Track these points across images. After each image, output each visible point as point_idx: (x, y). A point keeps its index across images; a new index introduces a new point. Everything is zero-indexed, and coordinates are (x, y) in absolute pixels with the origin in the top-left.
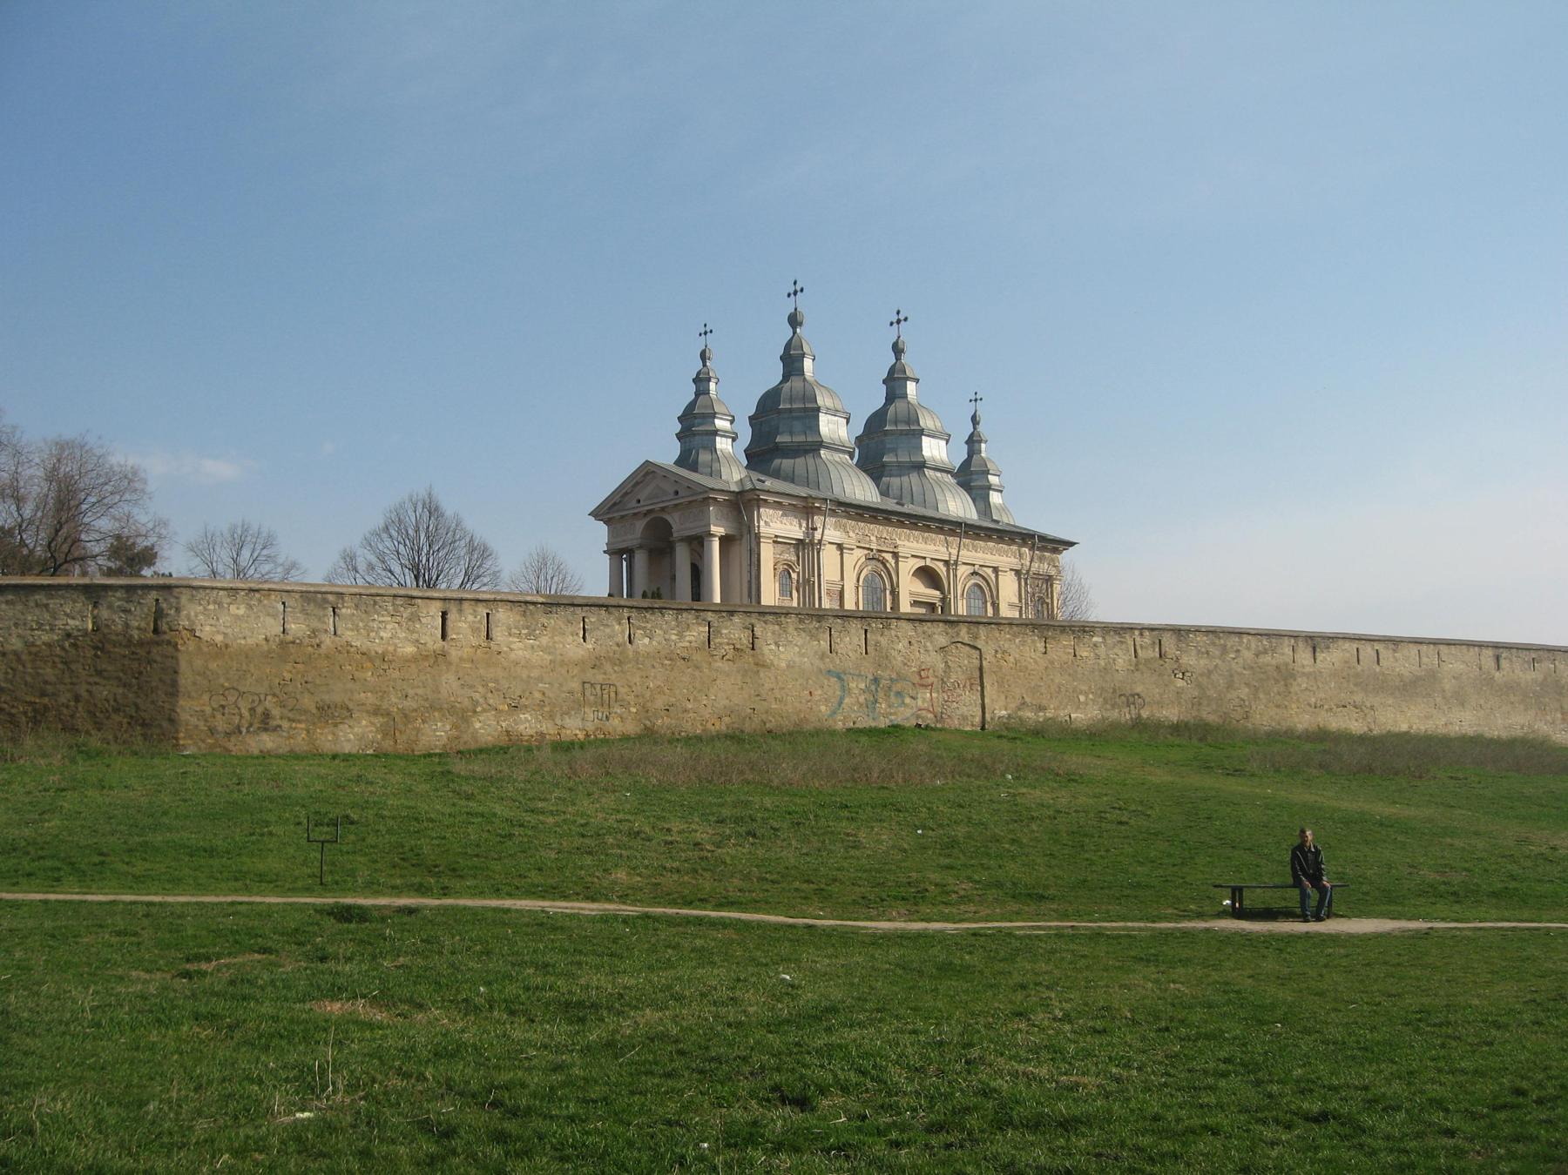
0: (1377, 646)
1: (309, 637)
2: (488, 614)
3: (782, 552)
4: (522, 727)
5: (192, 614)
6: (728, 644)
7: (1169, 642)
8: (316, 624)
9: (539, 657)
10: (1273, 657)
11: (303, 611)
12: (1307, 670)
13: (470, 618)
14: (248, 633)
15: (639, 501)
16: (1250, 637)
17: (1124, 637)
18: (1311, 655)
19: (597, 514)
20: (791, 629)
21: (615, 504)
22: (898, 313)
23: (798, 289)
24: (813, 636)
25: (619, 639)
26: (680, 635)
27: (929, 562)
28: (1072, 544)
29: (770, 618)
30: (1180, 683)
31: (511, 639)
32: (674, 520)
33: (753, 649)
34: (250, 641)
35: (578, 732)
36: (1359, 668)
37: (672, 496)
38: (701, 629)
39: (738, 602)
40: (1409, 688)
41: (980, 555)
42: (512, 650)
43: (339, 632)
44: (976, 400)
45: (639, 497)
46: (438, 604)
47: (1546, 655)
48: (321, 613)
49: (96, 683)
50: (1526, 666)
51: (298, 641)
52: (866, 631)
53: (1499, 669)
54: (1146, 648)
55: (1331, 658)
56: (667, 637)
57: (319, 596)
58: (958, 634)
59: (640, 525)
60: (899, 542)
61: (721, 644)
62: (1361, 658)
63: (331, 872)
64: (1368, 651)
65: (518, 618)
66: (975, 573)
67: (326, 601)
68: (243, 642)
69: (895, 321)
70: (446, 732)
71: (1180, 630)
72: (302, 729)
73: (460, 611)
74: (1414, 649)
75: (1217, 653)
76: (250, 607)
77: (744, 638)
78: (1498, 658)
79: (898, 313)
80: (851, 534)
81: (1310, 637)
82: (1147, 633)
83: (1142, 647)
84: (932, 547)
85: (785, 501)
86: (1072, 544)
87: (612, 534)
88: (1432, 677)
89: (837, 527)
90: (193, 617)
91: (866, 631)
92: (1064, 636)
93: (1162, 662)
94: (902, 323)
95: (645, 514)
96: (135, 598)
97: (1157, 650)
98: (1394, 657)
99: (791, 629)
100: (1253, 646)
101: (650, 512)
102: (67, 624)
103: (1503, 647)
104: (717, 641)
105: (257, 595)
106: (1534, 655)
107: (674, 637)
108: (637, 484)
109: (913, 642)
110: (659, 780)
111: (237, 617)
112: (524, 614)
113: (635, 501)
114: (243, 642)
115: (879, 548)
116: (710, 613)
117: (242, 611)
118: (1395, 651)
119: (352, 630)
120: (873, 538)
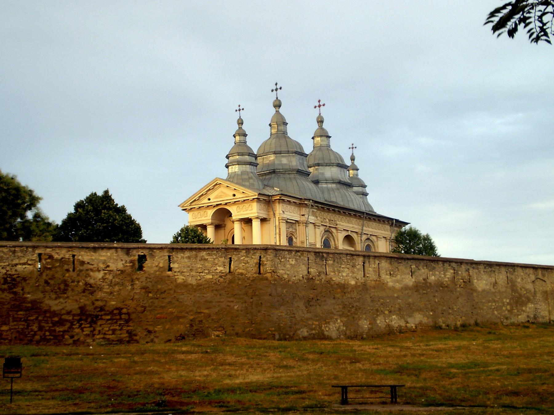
3: (289, 227)
6: (461, 279)
8: (320, 269)
9: (398, 286)
13: (373, 266)
14: (296, 274)
15: (209, 199)
22: (319, 101)
27: (349, 233)
32: (233, 209)
33: (470, 282)
41: (370, 229)
43: (328, 273)
44: (353, 148)
45: (209, 197)
49: (233, 302)
51: (314, 278)
59: (211, 212)
60: (338, 223)
66: (368, 239)
67: (323, 256)
69: (238, 109)
70: (368, 325)
72: (29, 293)
76: (296, 260)
79: (319, 101)
80: (319, 218)
84: (351, 225)
85: (292, 200)
89: (314, 214)
95: (214, 206)
101: (217, 205)
104: (457, 277)
110: (318, 331)
112: (390, 263)
113: (207, 198)
114: (294, 278)
115: (330, 226)
120: (327, 220)
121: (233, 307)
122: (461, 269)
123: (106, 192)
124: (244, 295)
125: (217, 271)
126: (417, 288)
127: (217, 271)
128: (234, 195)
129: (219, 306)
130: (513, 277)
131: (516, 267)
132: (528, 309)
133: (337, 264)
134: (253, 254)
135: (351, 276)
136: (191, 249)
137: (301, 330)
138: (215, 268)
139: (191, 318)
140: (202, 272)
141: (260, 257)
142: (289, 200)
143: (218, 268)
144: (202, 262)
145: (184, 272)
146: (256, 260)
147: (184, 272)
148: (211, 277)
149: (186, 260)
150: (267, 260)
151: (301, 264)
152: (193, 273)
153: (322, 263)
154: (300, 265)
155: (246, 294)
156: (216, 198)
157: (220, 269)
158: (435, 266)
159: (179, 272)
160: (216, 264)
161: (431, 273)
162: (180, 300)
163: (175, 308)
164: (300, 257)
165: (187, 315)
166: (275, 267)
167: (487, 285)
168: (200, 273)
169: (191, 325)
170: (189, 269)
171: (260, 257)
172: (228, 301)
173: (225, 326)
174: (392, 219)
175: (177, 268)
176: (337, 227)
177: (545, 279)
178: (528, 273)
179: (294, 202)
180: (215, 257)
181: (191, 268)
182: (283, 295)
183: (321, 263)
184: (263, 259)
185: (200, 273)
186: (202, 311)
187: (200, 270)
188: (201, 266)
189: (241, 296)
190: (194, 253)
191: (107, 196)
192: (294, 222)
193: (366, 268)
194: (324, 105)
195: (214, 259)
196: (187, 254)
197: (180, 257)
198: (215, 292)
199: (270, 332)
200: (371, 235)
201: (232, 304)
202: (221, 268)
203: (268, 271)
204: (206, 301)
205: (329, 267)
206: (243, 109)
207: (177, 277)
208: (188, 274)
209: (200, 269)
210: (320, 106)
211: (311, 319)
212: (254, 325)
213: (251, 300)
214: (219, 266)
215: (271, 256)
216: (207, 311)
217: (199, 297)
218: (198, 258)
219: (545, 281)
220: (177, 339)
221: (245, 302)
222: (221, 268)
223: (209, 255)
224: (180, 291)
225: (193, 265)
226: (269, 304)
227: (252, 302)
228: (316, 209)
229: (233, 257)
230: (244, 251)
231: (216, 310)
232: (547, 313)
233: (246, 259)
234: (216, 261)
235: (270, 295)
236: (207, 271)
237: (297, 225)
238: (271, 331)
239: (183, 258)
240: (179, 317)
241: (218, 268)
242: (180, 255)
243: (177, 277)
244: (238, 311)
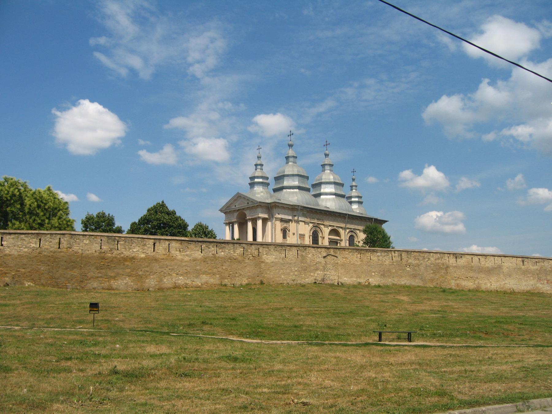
0: (479, 257)
1: (110, 251)
2: (169, 244)
4: (180, 282)
5: (71, 243)
6: (250, 254)
7: (404, 255)
8: (112, 247)
9: (187, 259)
10: (441, 260)
11: (108, 242)
12: (454, 265)
13: (164, 245)
14: (90, 249)
15: (236, 206)
16: (433, 254)
17: (388, 254)
18: (455, 260)
19: (221, 210)
20: (272, 250)
21: (228, 207)
22: (326, 142)
23: (292, 134)
24: (280, 253)
25: (213, 252)
26: (234, 252)
27: (335, 228)
28: (386, 221)
29: (265, 246)
30: (408, 269)
31: (177, 252)
32: (247, 212)
34: (90, 252)
35: (199, 283)
36: (473, 264)
37: (247, 205)
38: (241, 249)
39: (270, 241)
40: (489, 271)
42: (177, 256)
46: (153, 240)
47: (541, 260)
48: (114, 243)
49: (40, 265)
50: (534, 264)
52: (298, 251)
53: (523, 265)
54: (396, 257)
55: (462, 261)
56: (229, 252)
57: (113, 237)
58: (330, 252)
59: (236, 214)
61: (248, 255)
62: (473, 261)
63: (479, 357)
64: (476, 259)
65: (179, 245)
67: (115, 239)
68: (88, 252)
71: (408, 251)
73: (160, 243)
74: (492, 258)
75: (422, 259)
77: (256, 253)
78: (523, 261)
79: (326, 142)
81: (455, 254)
82: (396, 252)
83: (395, 257)
86: (386, 221)
87: (227, 218)
88: (500, 267)
90: (71, 244)
91: (298, 251)
92: (367, 253)
93: (401, 262)
94: (328, 145)
96: (53, 237)
97: (400, 258)
98: (485, 261)
99: (272, 250)
100: (435, 257)
102: (31, 246)
103: (525, 258)
105: (93, 237)
106: (537, 260)
107: (232, 252)
108: (235, 200)
109: (314, 254)
111: (86, 244)
113: (234, 206)
114: (88, 252)
116: (244, 244)
117: (87, 242)
118: (485, 258)
119: (124, 249)
121: (41, 268)
122: (251, 248)
123: (163, 202)
124: (48, 261)
125: (31, 247)
126: (204, 260)
127: (31, 247)
128: (248, 203)
129: (31, 267)
130: (304, 254)
131: (307, 248)
132: (316, 275)
133: (128, 244)
134: (55, 237)
135: (142, 251)
136: (15, 234)
137: (92, 283)
138: (30, 245)
139: (13, 274)
140: (21, 247)
141: (60, 238)
142: (282, 206)
143: (32, 245)
144: (22, 241)
145: (10, 247)
146: (57, 241)
147: (10, 247)
148: (27, 250)
149: (11, 240)
150: (65, 241)
151: (94, 243)
152: (16, 248)
153: (114, 243)
154: (93, 244)
155: (49, 260)
156: (239, 205)
157: (33, 245)
158: (225, 246)
159: (7, 246)
160: (31, 243)
161: (221, 250)
162: (7, 263)
163: (3, 267)
164: (93, 239)
165: (11, 272)
166: (70, 245)
167: (276, 258)
168: (20, 247)
169: (13, 278)
170: (13, 245)
171: (60, 238)
172: (37, 265)
173: (35, 279)
174: (372, 219)
175: (6, 244)
176: (324, 223)
177: (336, 255)
178: (320, 251)
179: (281, 207)
180: (30, 238)
181: (14, 244)
182: (76, 262)
183: (113, 243)
184: (62, 240)
185: (20, 247)
186: (20, 270)
187: (20, 246)
188: (21, 243)
189: (46, 262)
190: (17, 235)
191: (163, 205)
192: (288, 220)
193: (156, 246)
194: (329, 144)
195: (29, 239)
196: (13, 236)
197: (8, 238)
198: (29, 259)
199: (65, 284)
200: (354, 229)
201: (39, 267)
202: (34, 245)
203: (65, 247)
204: (23, 264)
205: (120, 245)
206: (261, 148)
207: (5, 250)
208: (13, 248)
209: (20, 245)
210: (327, 145)
211: (101, 277)
212: (54, 279)
213: (53, 264)
214: (33, 244)
215: (67, 238)
216: (23, 270)
217: (19, 262)
218: (19, 239)
219: (337, 257)
220: (4, 286)
221: (49, 266)
222: (34, 245)
223: (26, 237)
224: (6, 258)
225: (16, 243)
226: (65, 267)
227: (53, 266)
228: (306, 212)
229: (42, 238)
230: (49, 235)
231: (28, 270)
232: (336, 278)
233: (50, 240)
234: (31, 241)
235: (65, 262)
236: (24, 247)
237: (290, 222)
238: (65, 283)
239: (9, 238)
240: (6, 273)
241: (32, 245)
242: (8, 237)
243: (5, 250)
244: (43, 270)
